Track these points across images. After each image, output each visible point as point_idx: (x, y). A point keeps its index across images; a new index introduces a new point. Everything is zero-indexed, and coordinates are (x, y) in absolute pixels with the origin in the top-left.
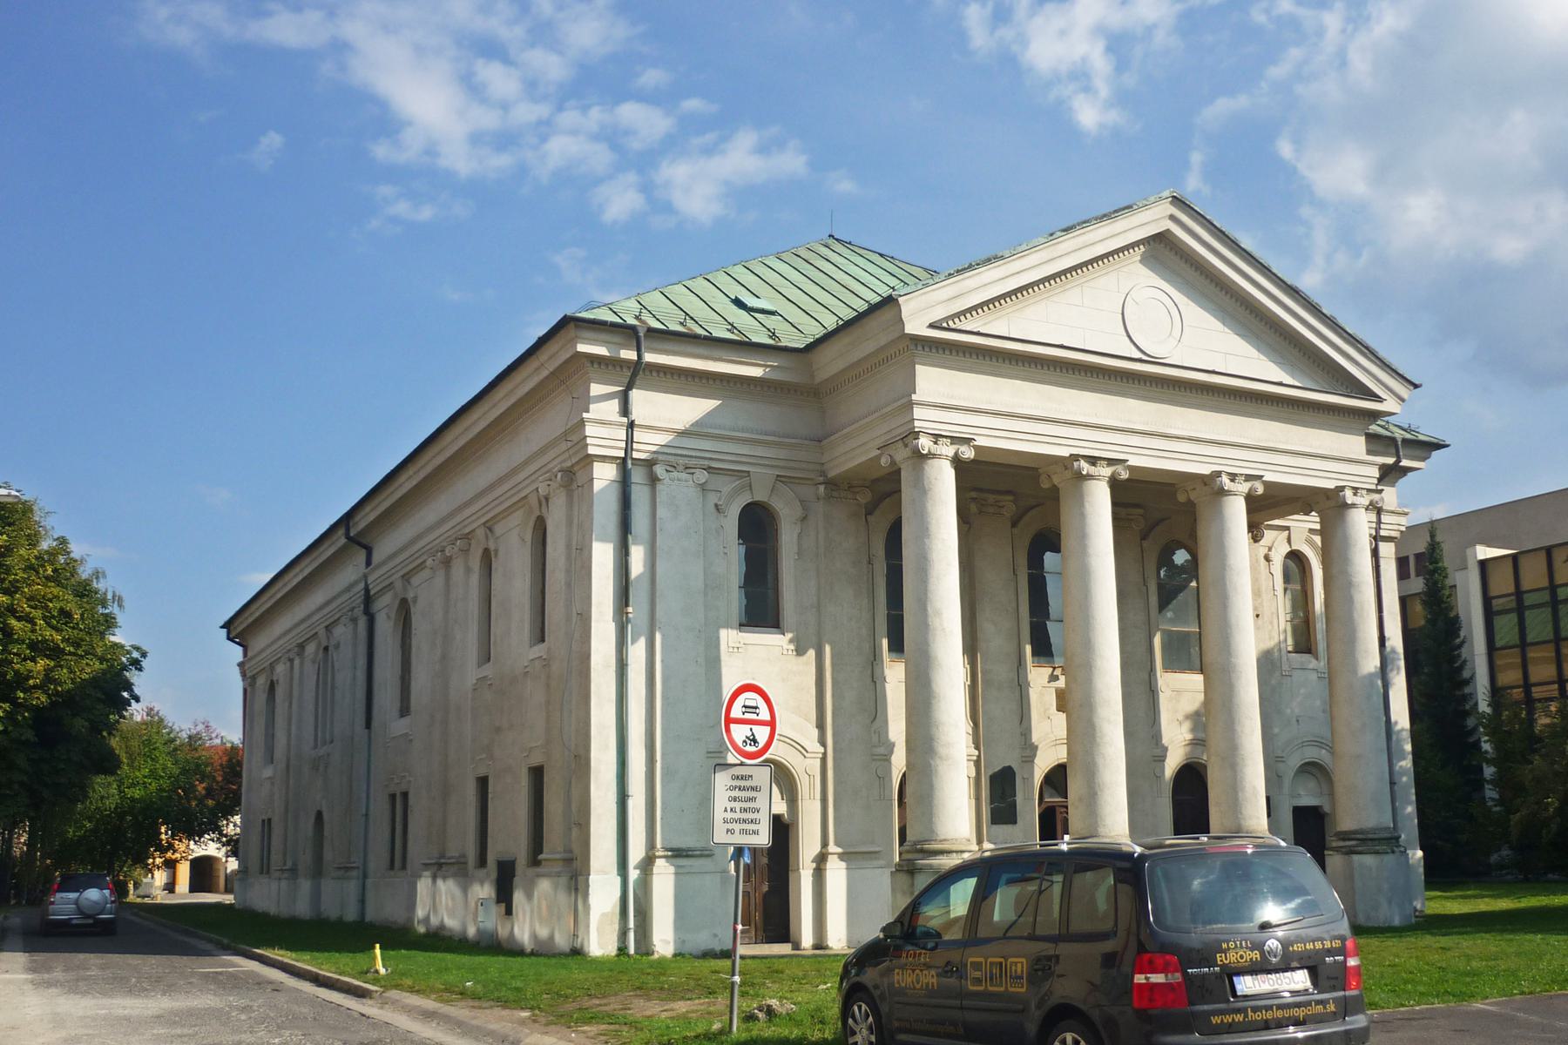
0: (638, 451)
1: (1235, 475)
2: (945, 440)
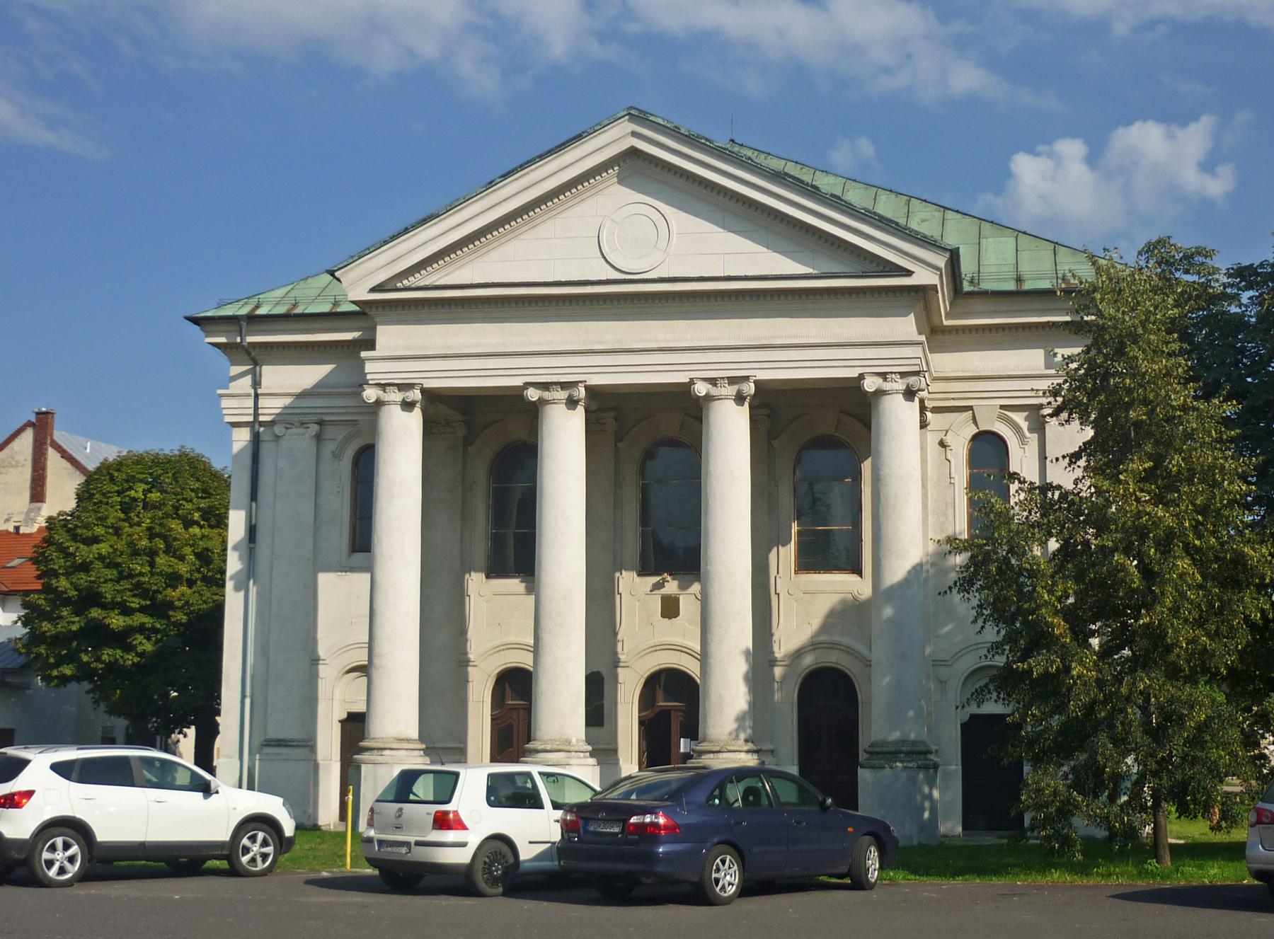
1: (715, 379)
2: (391, 388)
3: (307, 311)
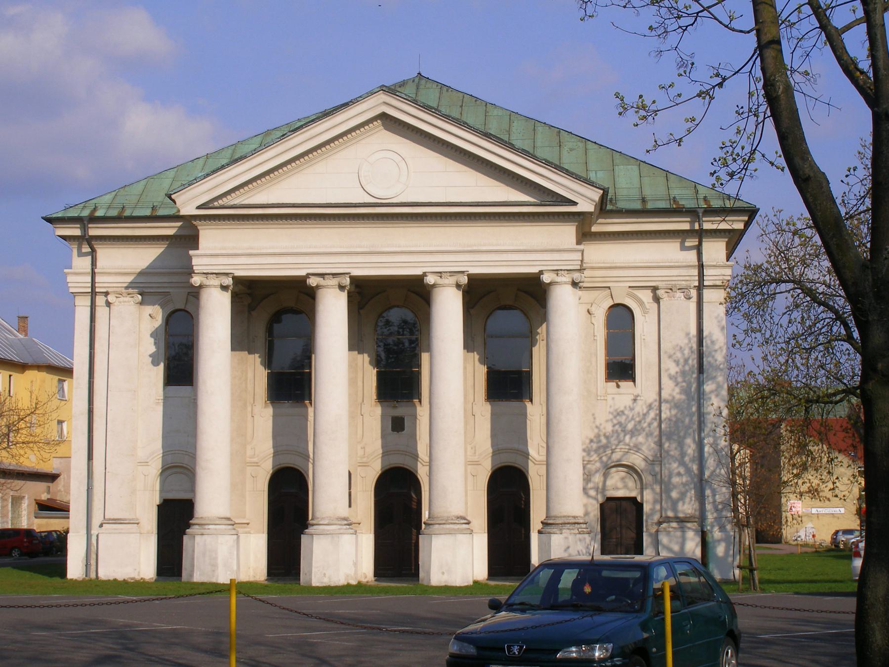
1: (440, 273)
3: (133, 215)
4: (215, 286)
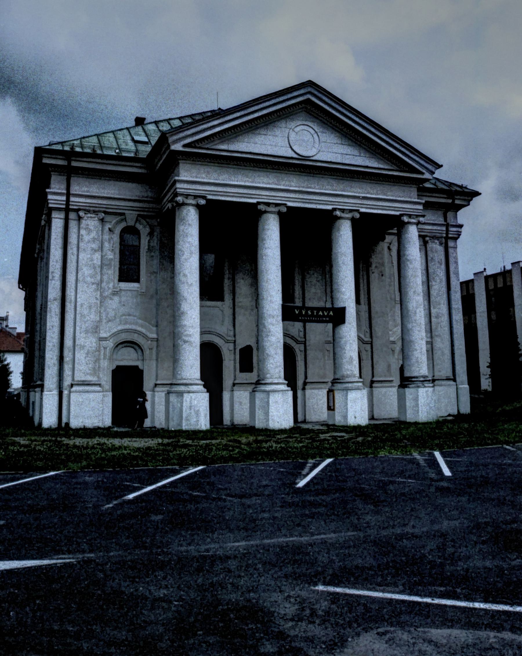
0: (73, 205)
4: (193, 205)
